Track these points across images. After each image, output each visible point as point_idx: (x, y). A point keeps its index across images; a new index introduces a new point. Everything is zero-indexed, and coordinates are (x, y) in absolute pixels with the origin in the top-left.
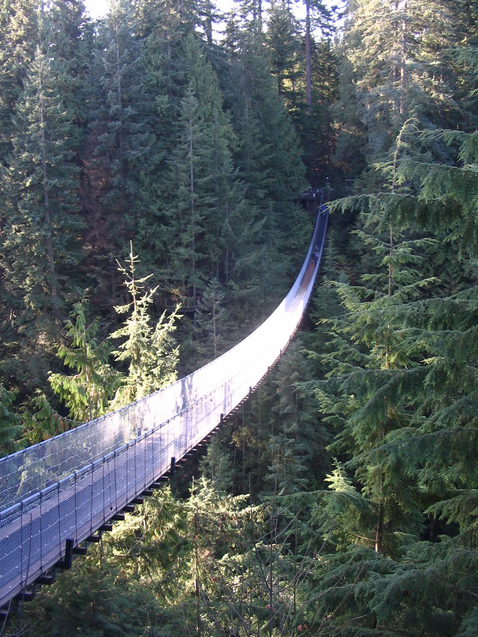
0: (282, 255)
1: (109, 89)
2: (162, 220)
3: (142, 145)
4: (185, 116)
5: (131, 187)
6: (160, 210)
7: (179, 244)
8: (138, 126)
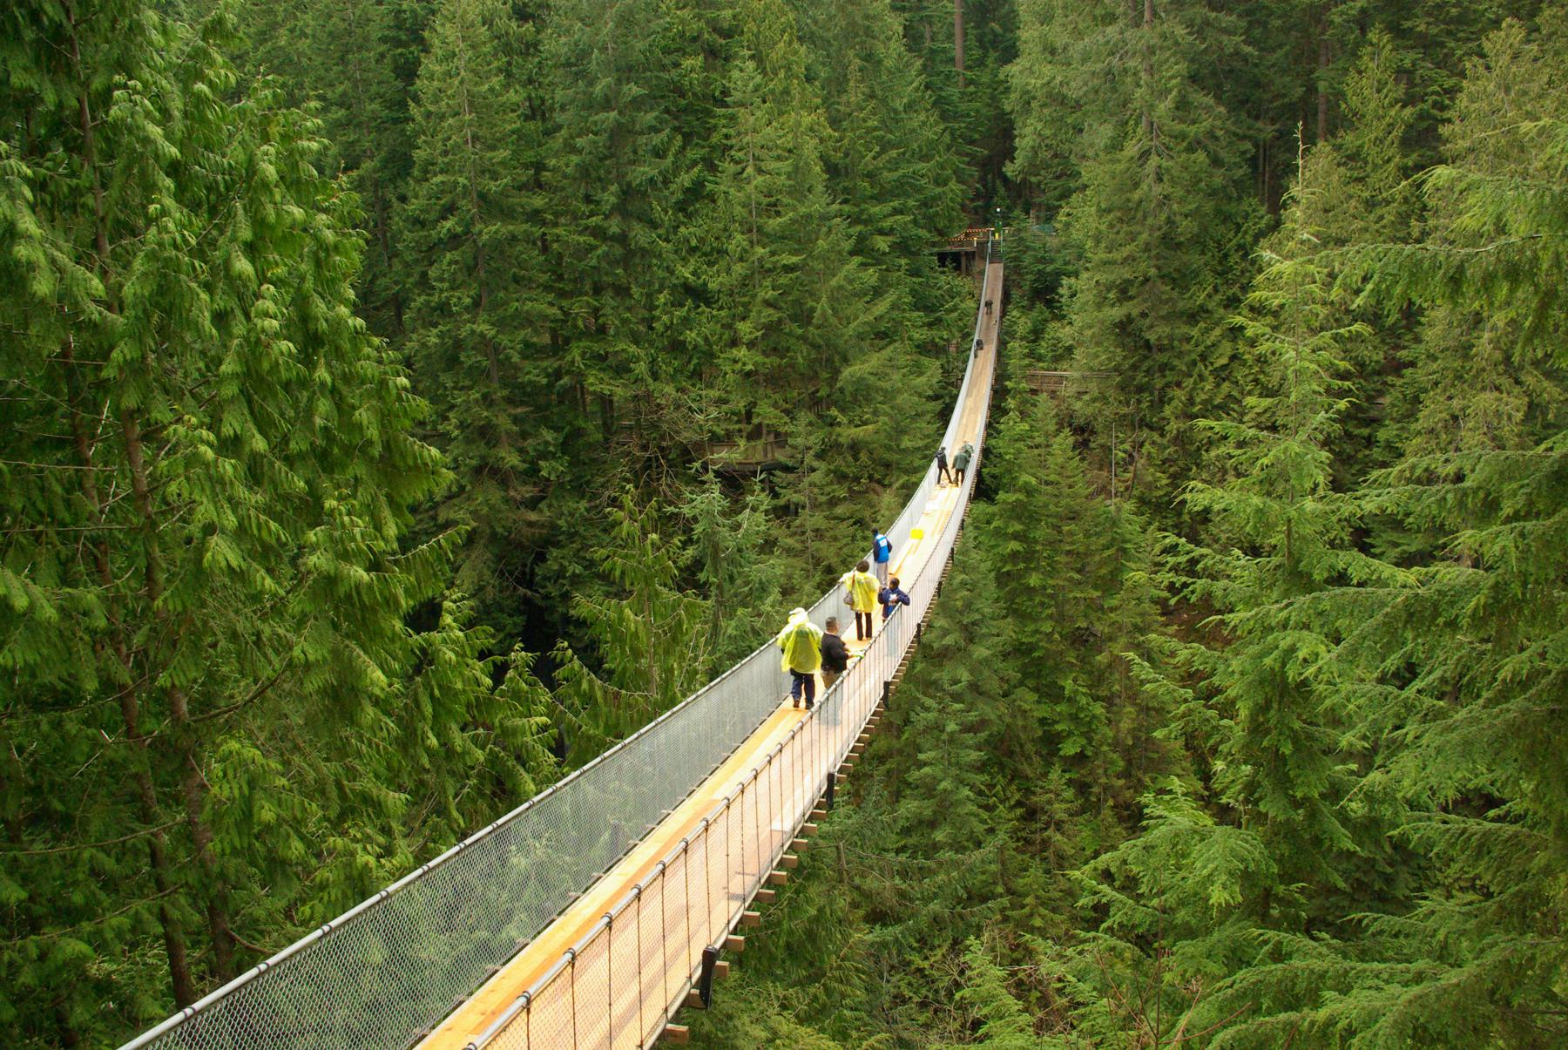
0: (925, 361)
2: (697, 294)
3: (658, 156)
4: (737, 96)
5: (641, 235)
6: (694, 273)
7: (734, 343)
8: (649, 118)
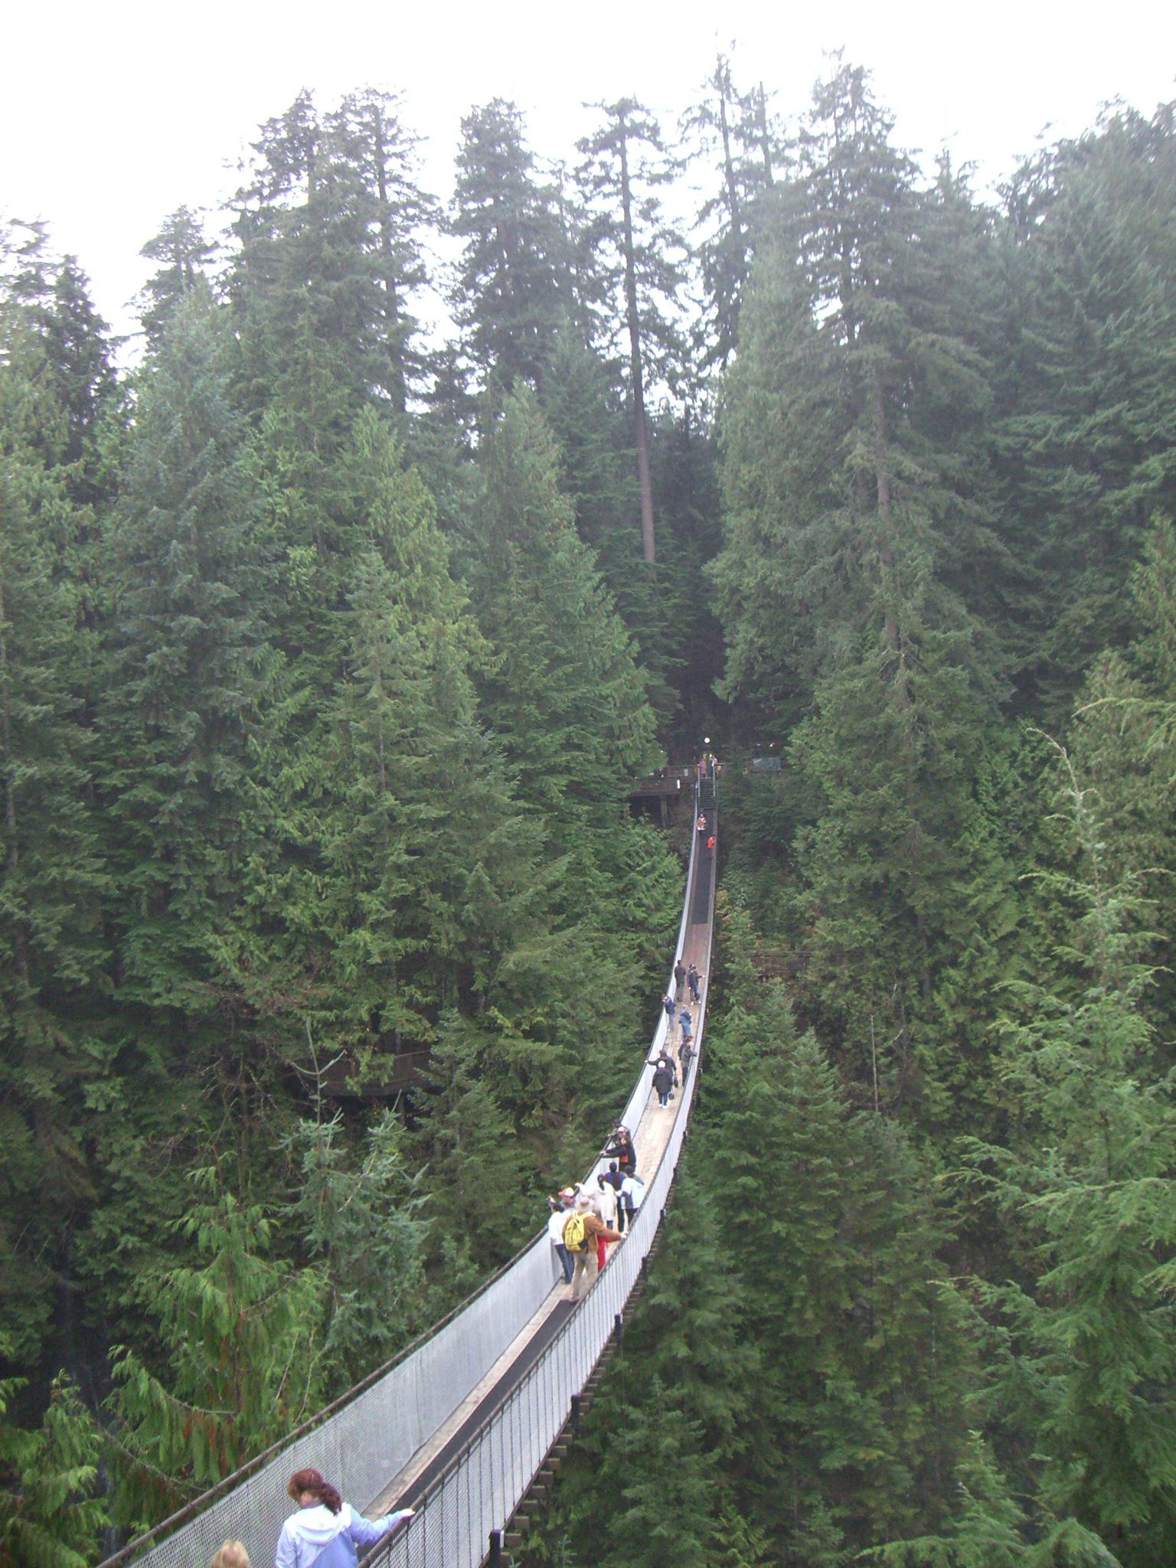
1: (171, 536)
6: (301, 828)
